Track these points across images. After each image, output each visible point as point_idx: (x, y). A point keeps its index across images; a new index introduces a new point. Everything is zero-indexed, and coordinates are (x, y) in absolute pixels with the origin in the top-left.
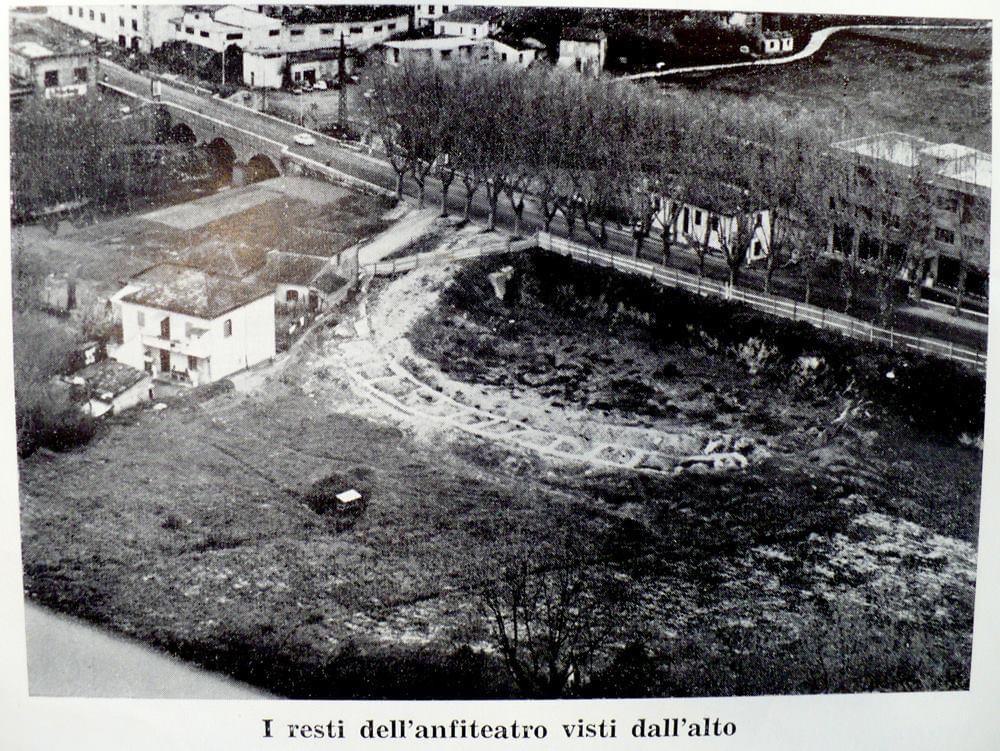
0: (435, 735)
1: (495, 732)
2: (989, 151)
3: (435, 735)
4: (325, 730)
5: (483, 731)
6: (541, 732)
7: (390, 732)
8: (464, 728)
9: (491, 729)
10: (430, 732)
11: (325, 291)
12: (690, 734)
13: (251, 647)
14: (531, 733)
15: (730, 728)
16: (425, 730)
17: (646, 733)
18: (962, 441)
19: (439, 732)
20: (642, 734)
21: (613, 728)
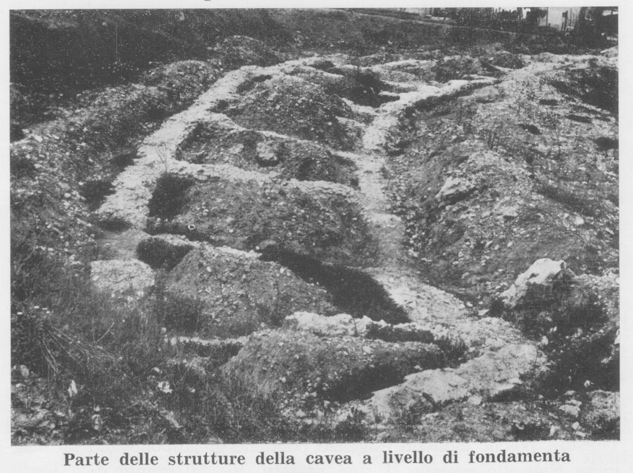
0: (520, 460)
1: (343, 459)
2: (614, 111)
3: (520, 460)
4: (176, 460)
5: (102, 460)
6: (349, 460)
7: (412, 459)
8: (391, 456)
9: (313, 457)
10: (517, 458)
11: (441, 185)
12: (77, 464)
13: (545, 349)
14: (190, 461)
15: (428, 459)
16: (514, 456)
17: (506, 460)
18: (76, 391)
19: (548, 457)
20: (504, 460)
21: (456, 456)
